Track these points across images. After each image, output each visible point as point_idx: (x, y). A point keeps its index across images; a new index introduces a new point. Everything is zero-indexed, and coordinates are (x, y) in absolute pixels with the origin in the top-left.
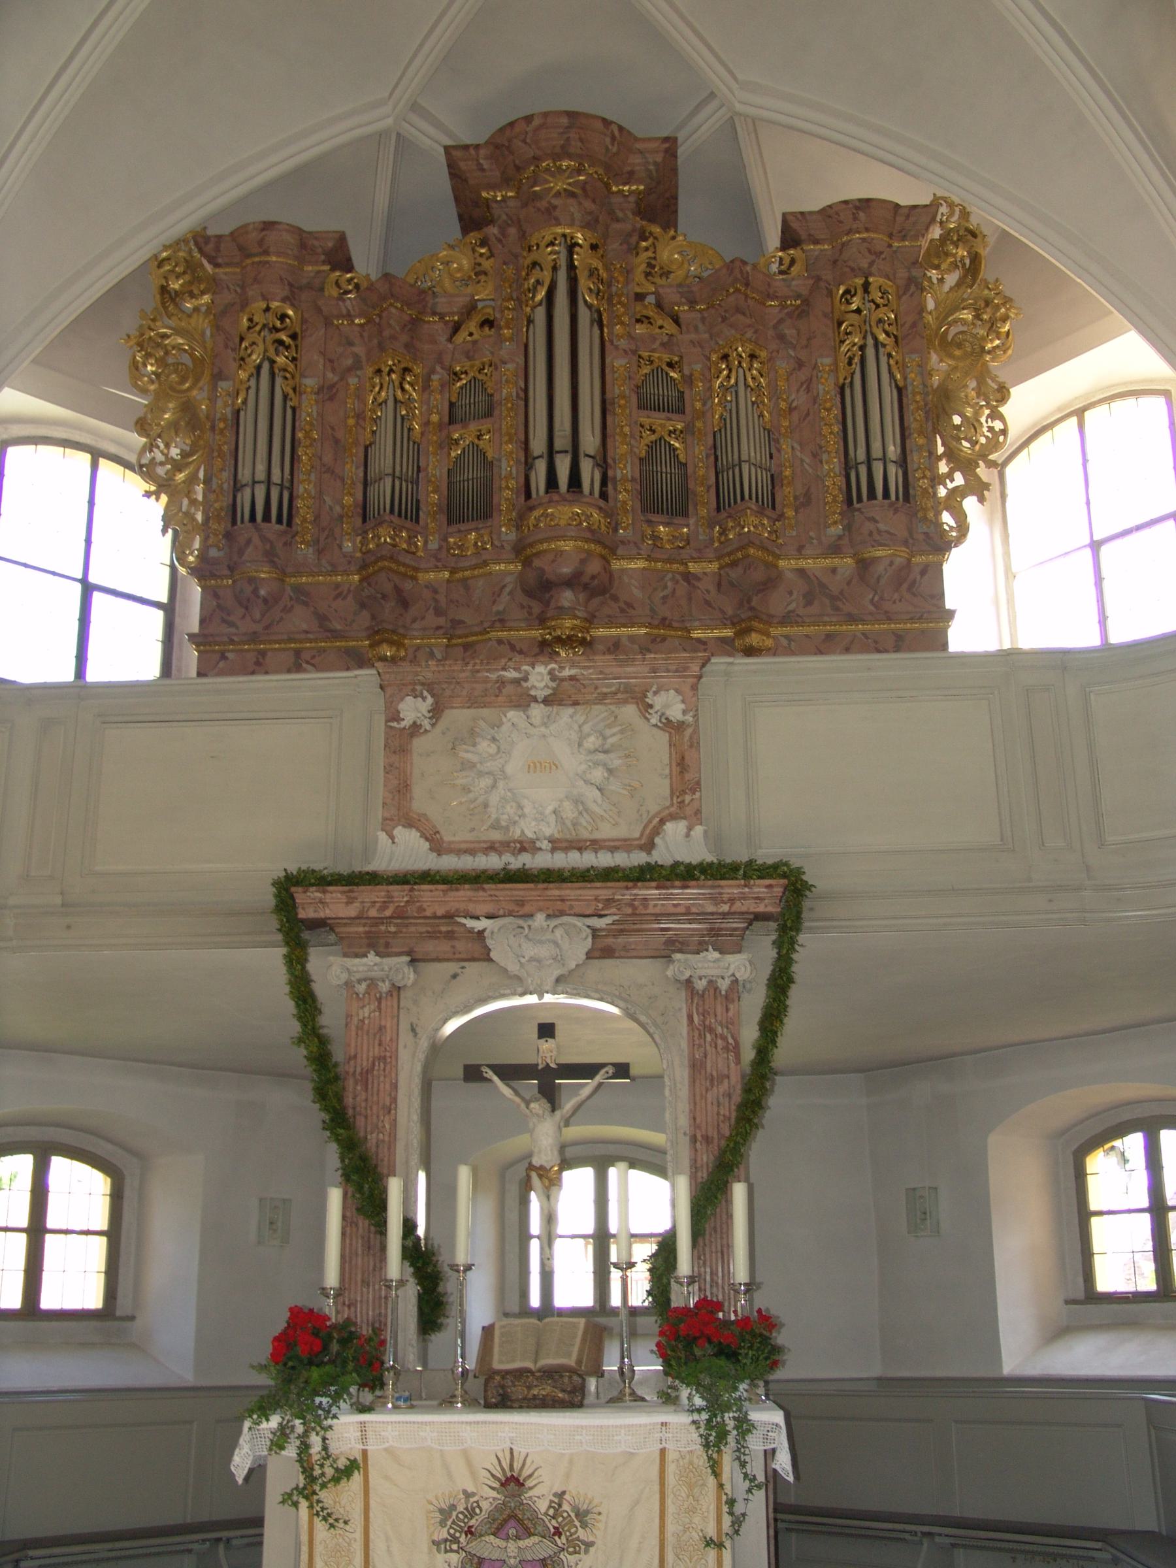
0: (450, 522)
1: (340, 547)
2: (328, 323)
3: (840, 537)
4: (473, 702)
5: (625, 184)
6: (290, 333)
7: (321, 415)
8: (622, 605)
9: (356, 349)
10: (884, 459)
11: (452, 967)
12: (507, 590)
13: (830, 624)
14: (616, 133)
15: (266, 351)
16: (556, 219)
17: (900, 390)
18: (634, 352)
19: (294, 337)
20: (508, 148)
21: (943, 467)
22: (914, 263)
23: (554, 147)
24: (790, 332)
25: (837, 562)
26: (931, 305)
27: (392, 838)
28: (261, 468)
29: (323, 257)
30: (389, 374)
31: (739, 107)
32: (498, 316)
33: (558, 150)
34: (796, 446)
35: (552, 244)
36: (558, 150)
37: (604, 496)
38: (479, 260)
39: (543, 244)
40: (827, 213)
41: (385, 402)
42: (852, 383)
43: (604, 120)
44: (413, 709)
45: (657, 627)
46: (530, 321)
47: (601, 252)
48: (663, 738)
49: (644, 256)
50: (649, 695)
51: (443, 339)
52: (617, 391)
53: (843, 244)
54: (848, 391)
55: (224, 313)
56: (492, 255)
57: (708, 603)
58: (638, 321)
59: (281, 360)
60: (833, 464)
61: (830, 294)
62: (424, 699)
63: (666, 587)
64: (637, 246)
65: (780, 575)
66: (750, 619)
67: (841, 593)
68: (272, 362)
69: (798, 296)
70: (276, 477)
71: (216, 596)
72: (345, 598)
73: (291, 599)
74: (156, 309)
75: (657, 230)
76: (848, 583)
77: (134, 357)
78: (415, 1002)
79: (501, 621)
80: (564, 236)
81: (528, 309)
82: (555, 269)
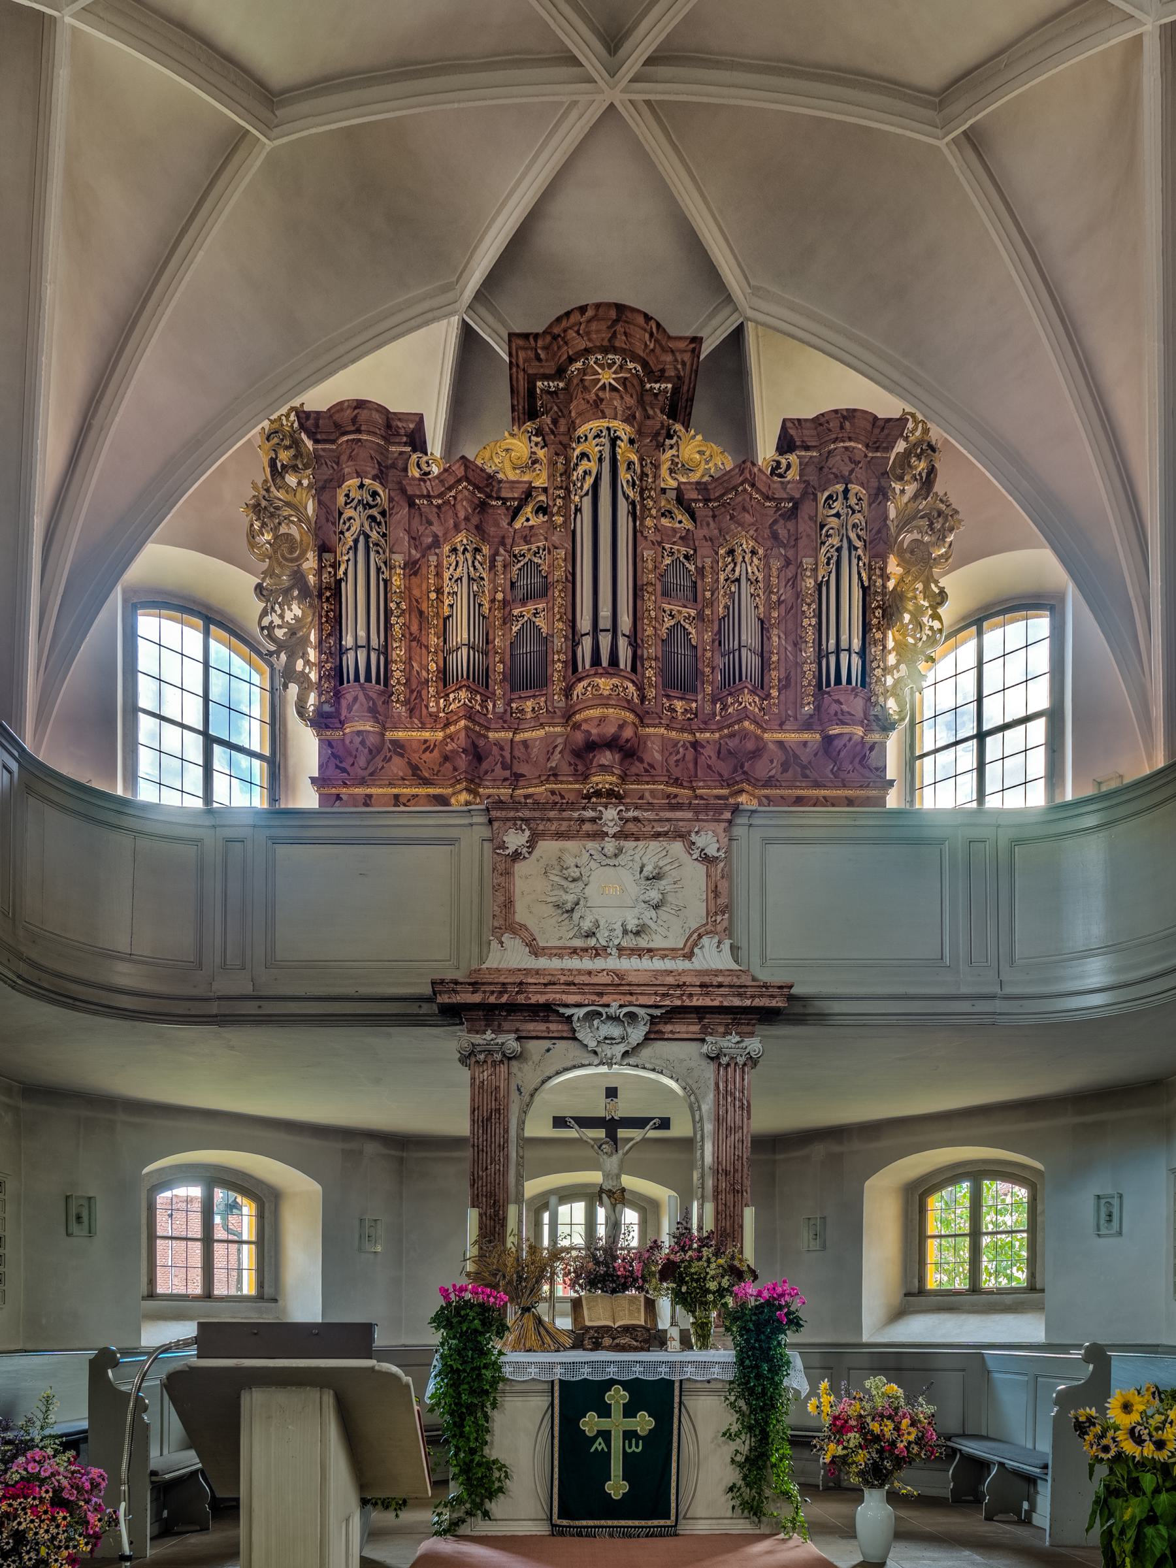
0: (512, 690)
1: (427, 707)
2: (412, 504)
3: (811, 716)
4: (560, 835)
5: (656, 382)
6: (380, 509)
7: (409, 588)
8: (646, 765)
9: (434, 528)
10: (849, 650)
11: (547, 1044)
12: (559, 749)
13: (801, 788)
14: (654, 330)
15: (362, 526)
16: (603, 412)
17: (865, 590)
18: (659, 543)
19: (383, 513)
20: (563, 339)
21: (892, 659)
22: (883, 474)
23: (603, 340)
24: (783, 533)
25: (806, 736)
26: (892, 514)
27: (502, 943)
28: (362, 633)
29: (405, 439)
30: (463, 553)
31: (750, 313)
32: (551, 503)
33: (606, 343)
34: (782, 636)
35: (598, 436)
36: (606, 343)
37: (634, 669)
38: (535, 449)
39: (590, 436)
40: (819, 421)
41: (461, 579)
42: (828, 581)
43: (646, 316)
44: (515, 840)
45: (672, 785)
46: (578, 510)
47: (636, 446)
48: (701, 869)
49: (669, 453)
50: (693, 835)
51: (504, 524)
52: (645, 579)
53: (829, 452)
54: (824, 589)
55: (323, 488)
56: (546, 445)
57: (709, 767)
58: (663, 515)
59: (374, 535)
60: (809, 652)
61: (815, 499)
62: (523, 831)
63: (678, 752)
64: (663, 445)
65: (766, 744)
66: (742, 781)
67: (810, 762)
68: (367, 537)
69: (791, 499)
70: (374, 643)
71: (330, 745)
72: (431, 752)
73: (390, 750)
74: (266, 481)
75: (678, 427)
76: (816, 755)
77: (252, 525)
78: (520, 1069)
79: (555, 775)
80: (608, 429)
81: (577, 499)
82: (600, 460)
